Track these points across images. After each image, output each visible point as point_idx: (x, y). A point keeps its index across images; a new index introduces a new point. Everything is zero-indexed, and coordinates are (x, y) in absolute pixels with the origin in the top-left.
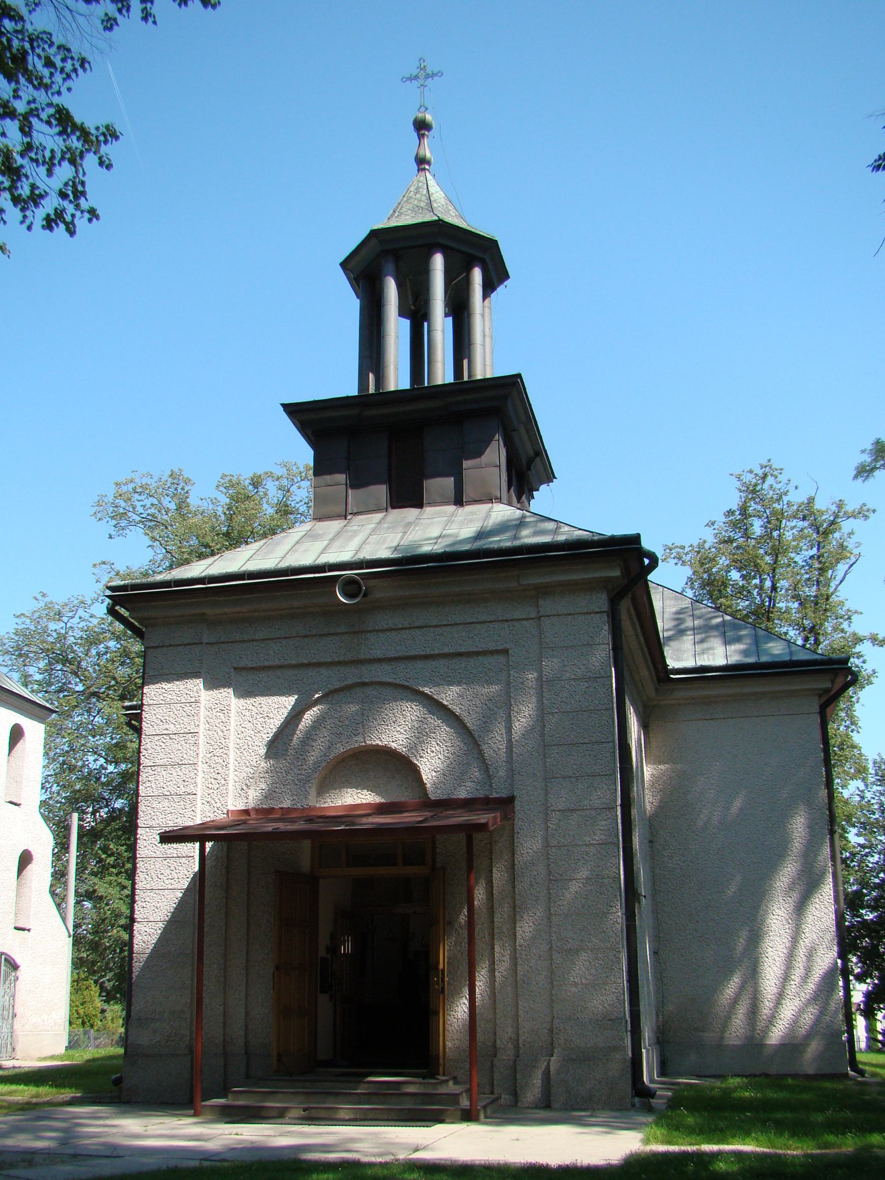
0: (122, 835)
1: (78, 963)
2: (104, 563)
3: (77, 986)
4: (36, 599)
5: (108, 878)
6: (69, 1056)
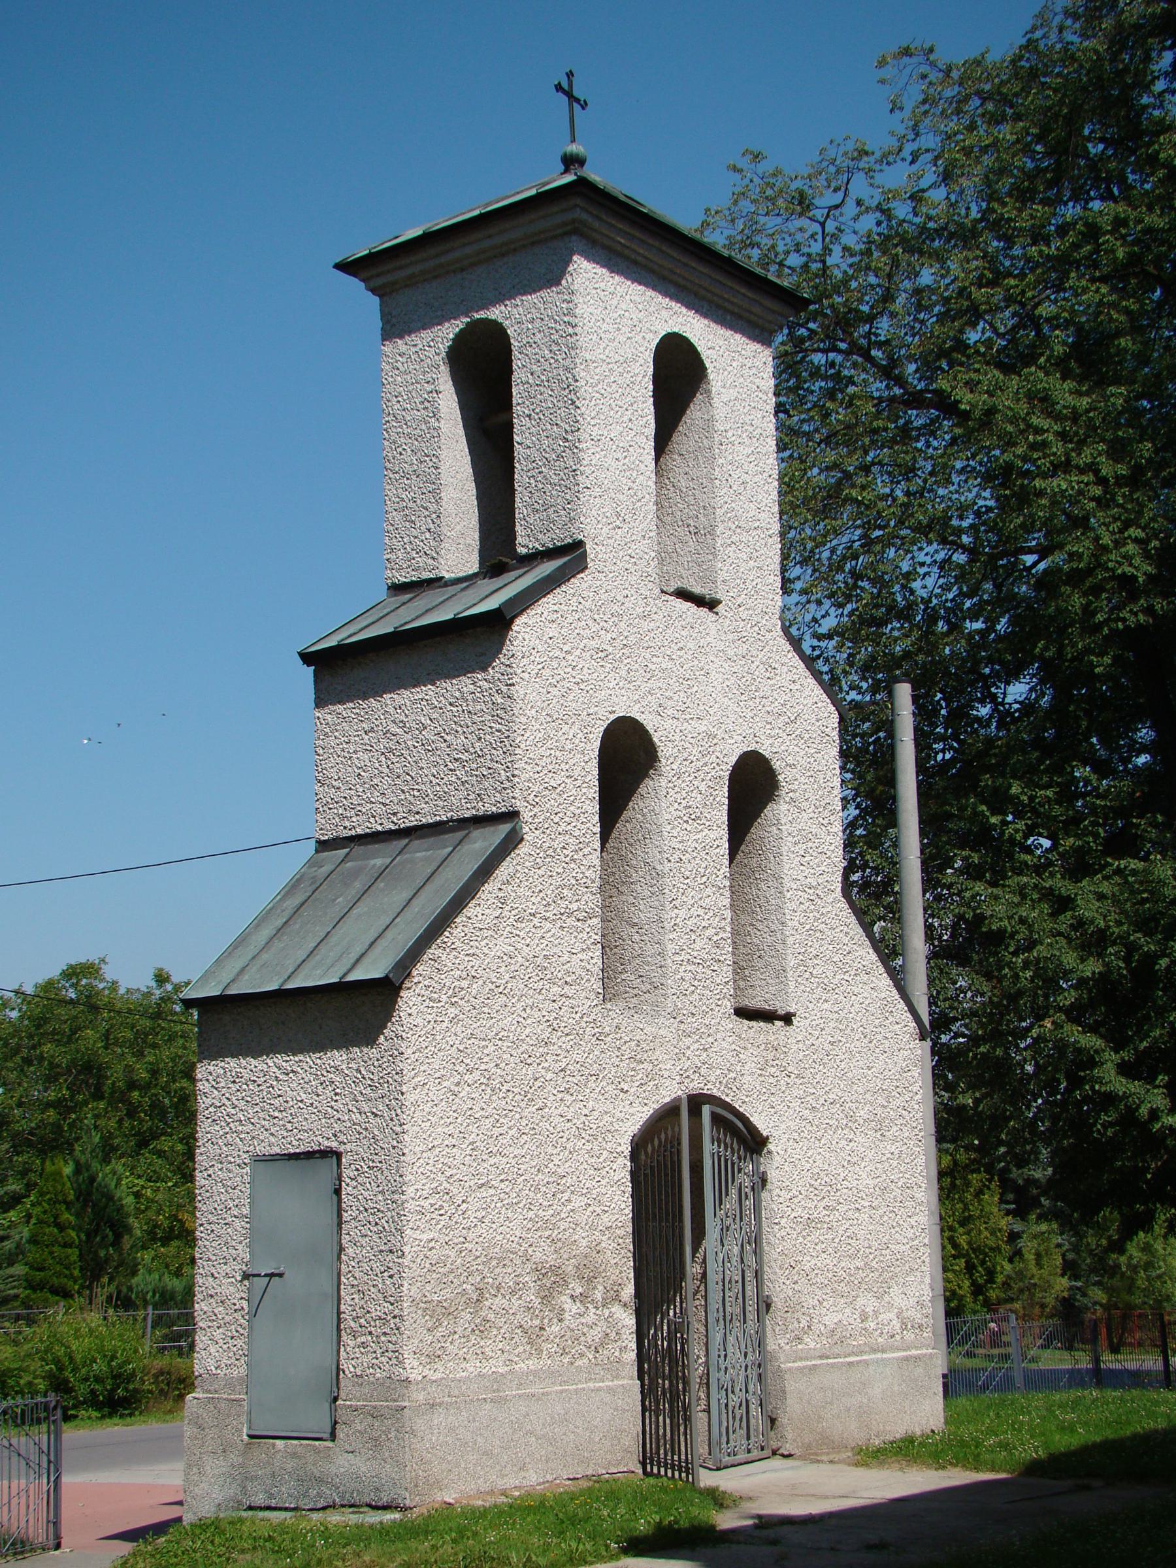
0: (1040, 761)
1: (950, 1126)
2: (907, 52)
3: (951, 1182)
4: (735, 169)
5: (1014, 881)
6: (963, 1444)
